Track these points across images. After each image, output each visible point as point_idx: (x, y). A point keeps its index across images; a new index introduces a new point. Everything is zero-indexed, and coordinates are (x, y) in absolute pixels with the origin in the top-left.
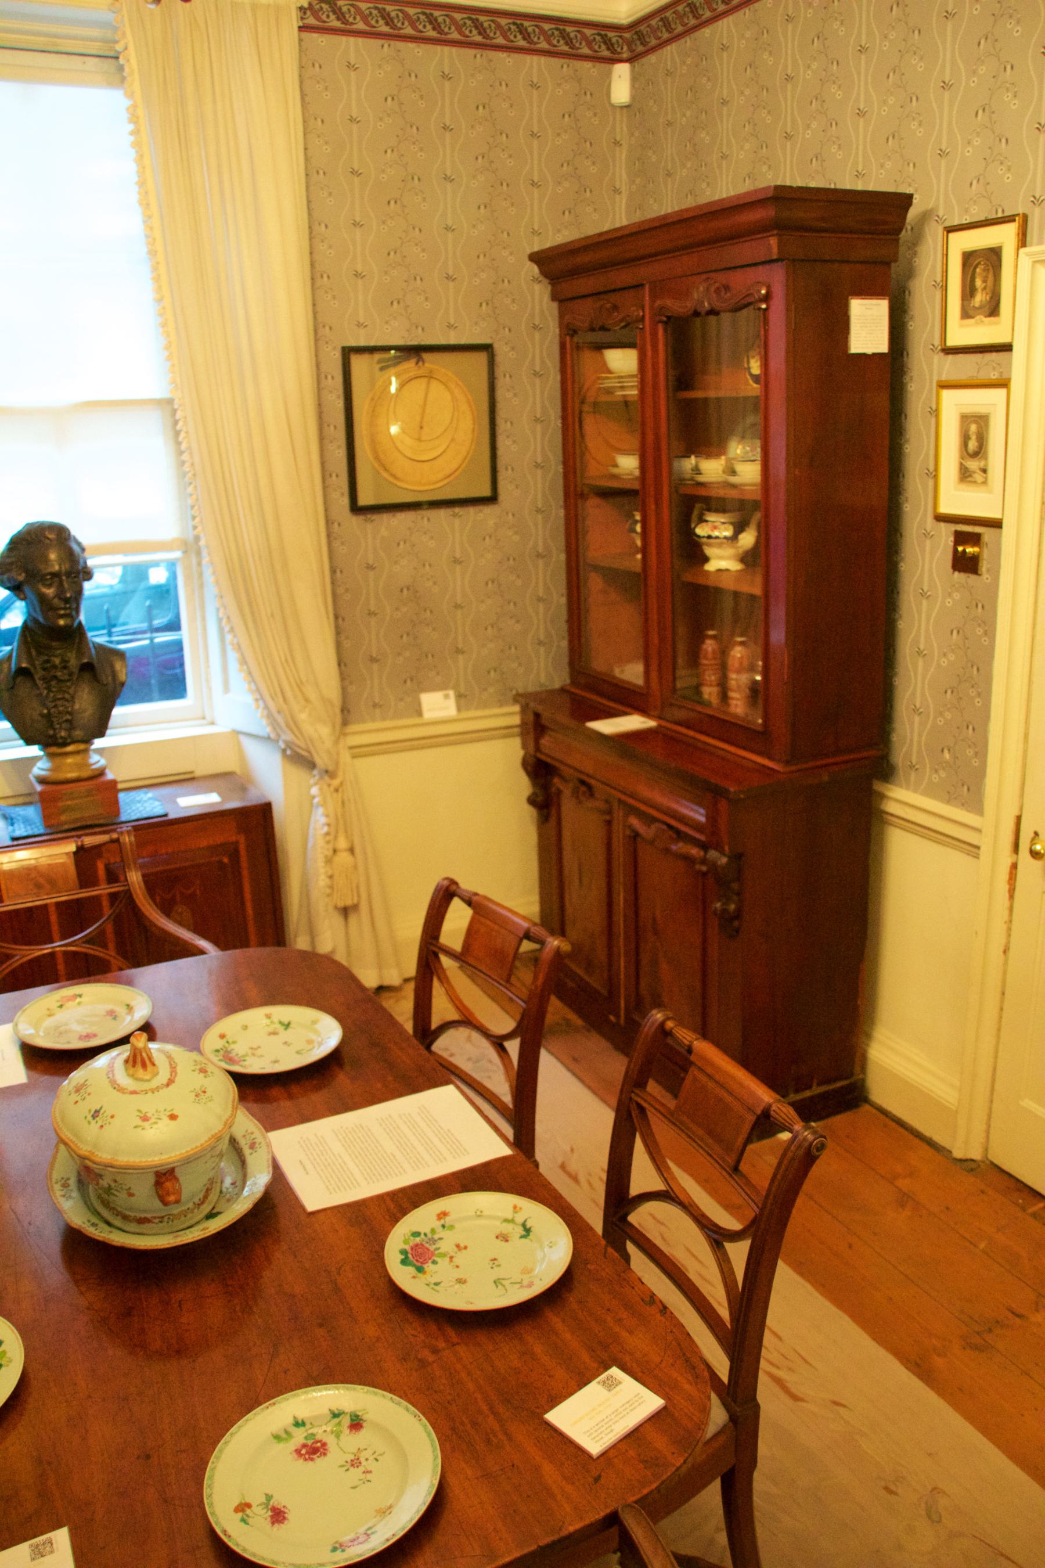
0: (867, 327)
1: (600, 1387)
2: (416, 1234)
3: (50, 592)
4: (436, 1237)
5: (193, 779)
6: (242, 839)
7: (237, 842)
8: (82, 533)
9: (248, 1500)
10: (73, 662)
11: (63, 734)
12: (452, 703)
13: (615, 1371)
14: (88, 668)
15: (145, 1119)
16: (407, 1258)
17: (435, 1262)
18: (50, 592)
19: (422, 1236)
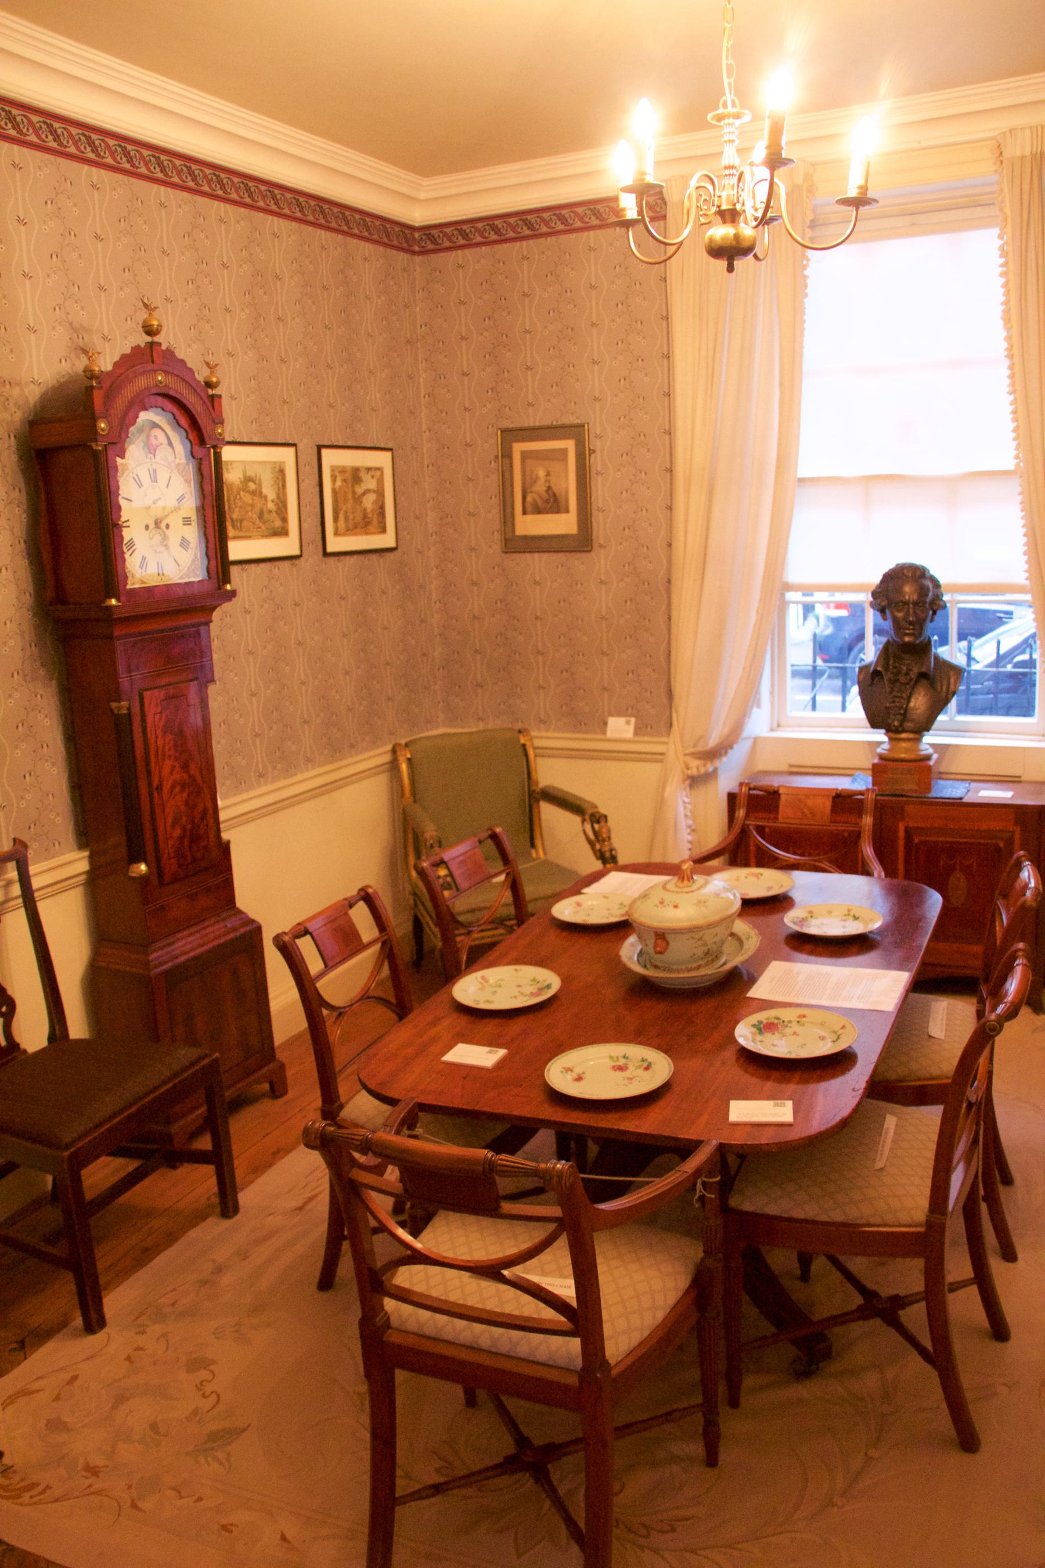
2: (779, 1019)
3: (900, 615)
5: (1020, 782)
6: (1018, 830)
7: (1013, 832)
8: (941, 571)
10: (915, 671)
11: (896, 723)
14: (924, 676)
15: (661, 903)
18: (900, 615)
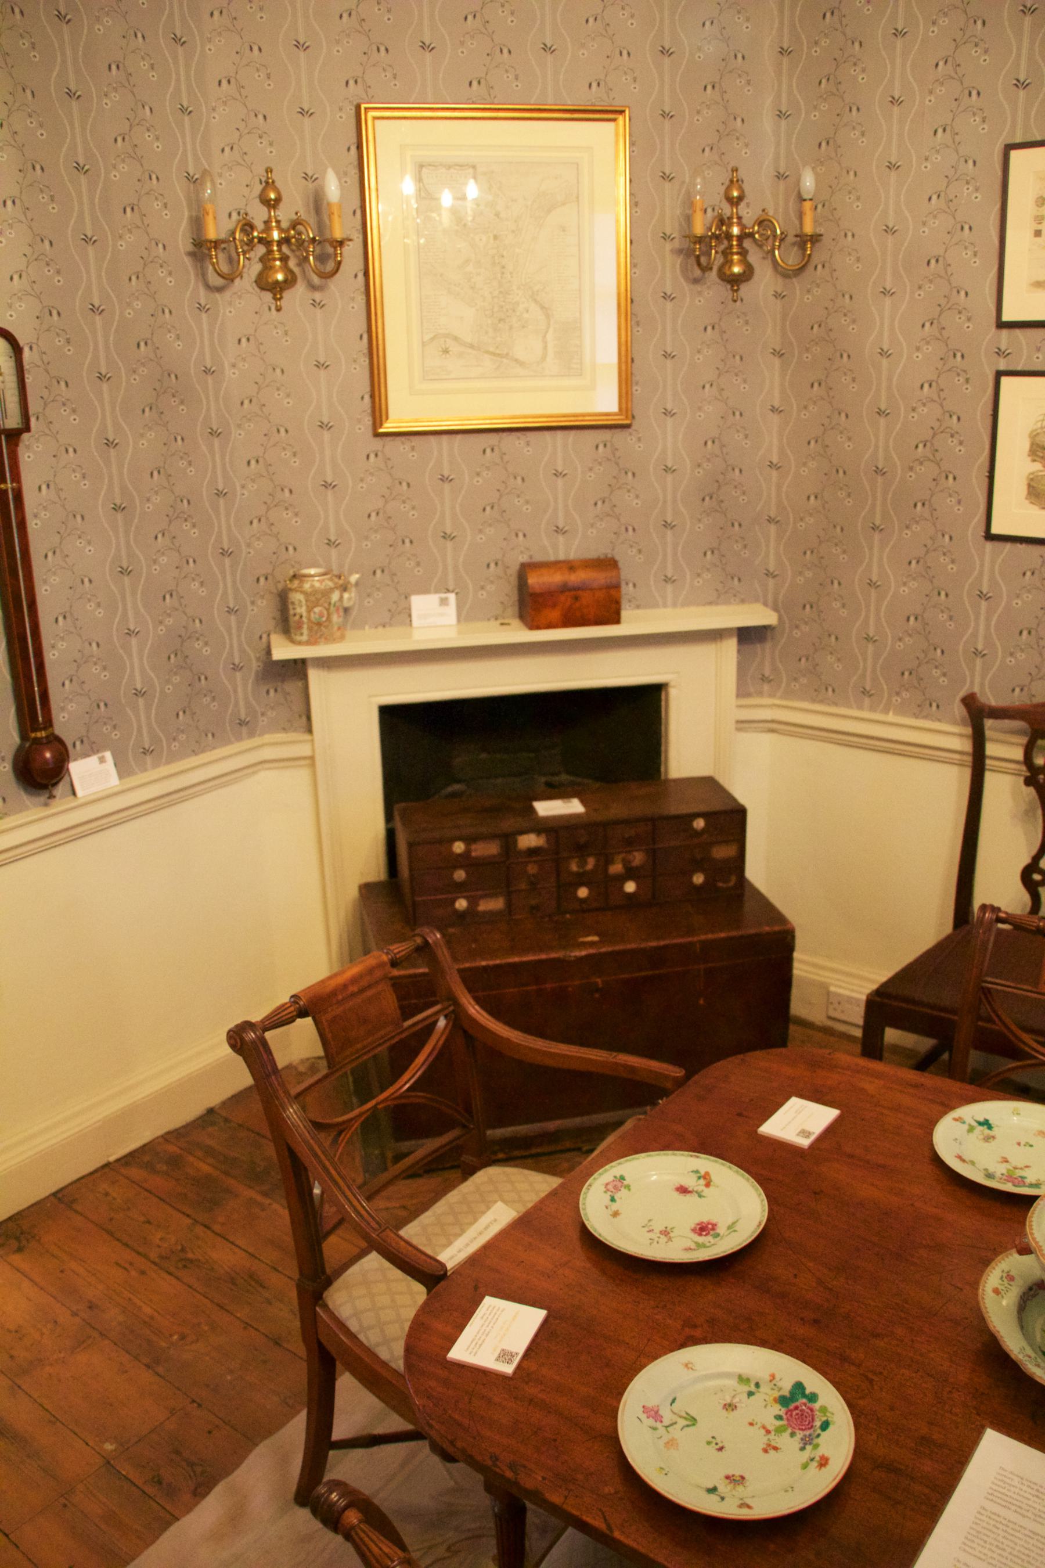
0: (699, 824)
1: (514, 1350)
2: (825, 1426)
4: (809, 1448)
9: (711, 1188)
12: (451, 612)
13: (508, 1369)
16: (804, 1395)
17: (779, 1417)
19: (819, 1431)
